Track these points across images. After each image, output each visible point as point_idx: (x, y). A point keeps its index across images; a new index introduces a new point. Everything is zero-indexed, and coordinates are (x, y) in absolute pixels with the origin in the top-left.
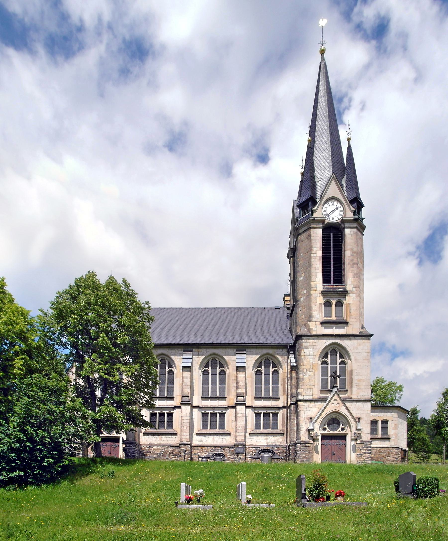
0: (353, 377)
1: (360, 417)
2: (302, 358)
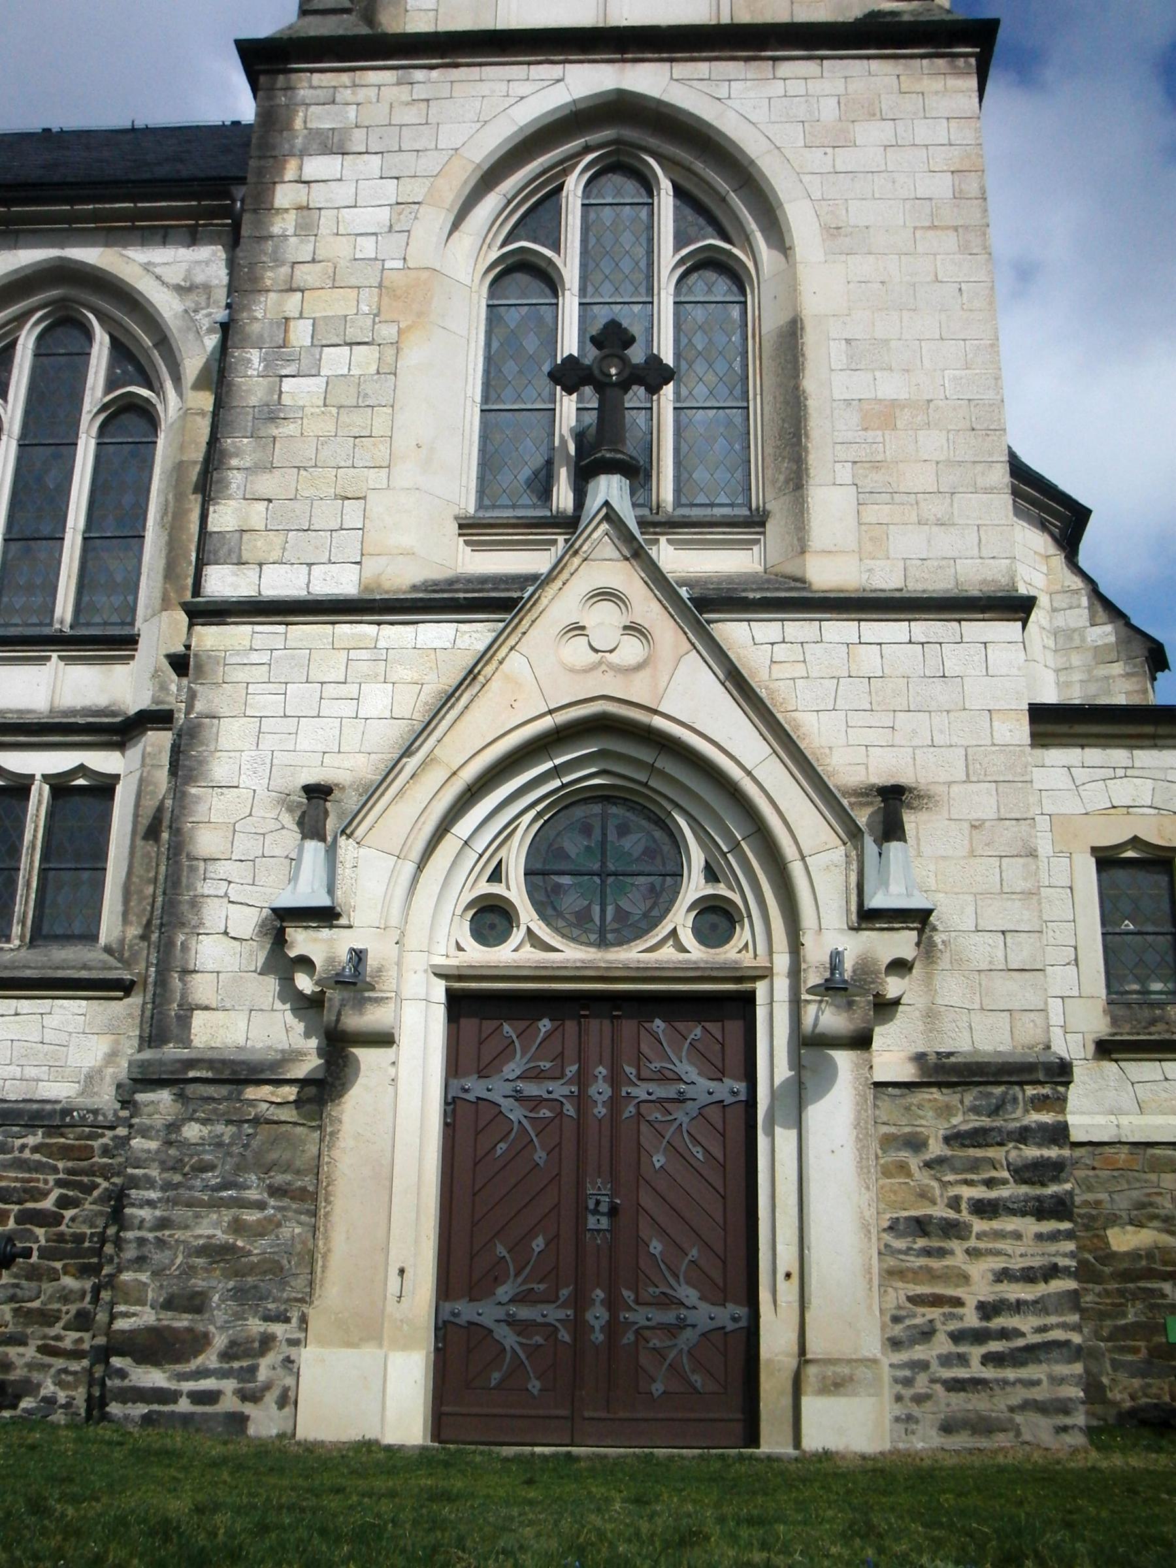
0: (810, 383)
1: (905, 779)
2: (283, 225)
